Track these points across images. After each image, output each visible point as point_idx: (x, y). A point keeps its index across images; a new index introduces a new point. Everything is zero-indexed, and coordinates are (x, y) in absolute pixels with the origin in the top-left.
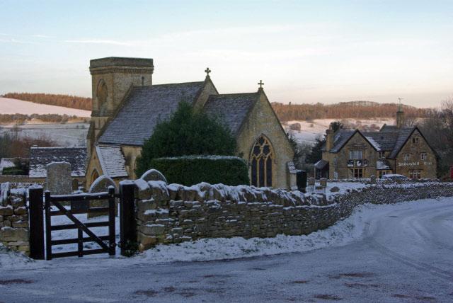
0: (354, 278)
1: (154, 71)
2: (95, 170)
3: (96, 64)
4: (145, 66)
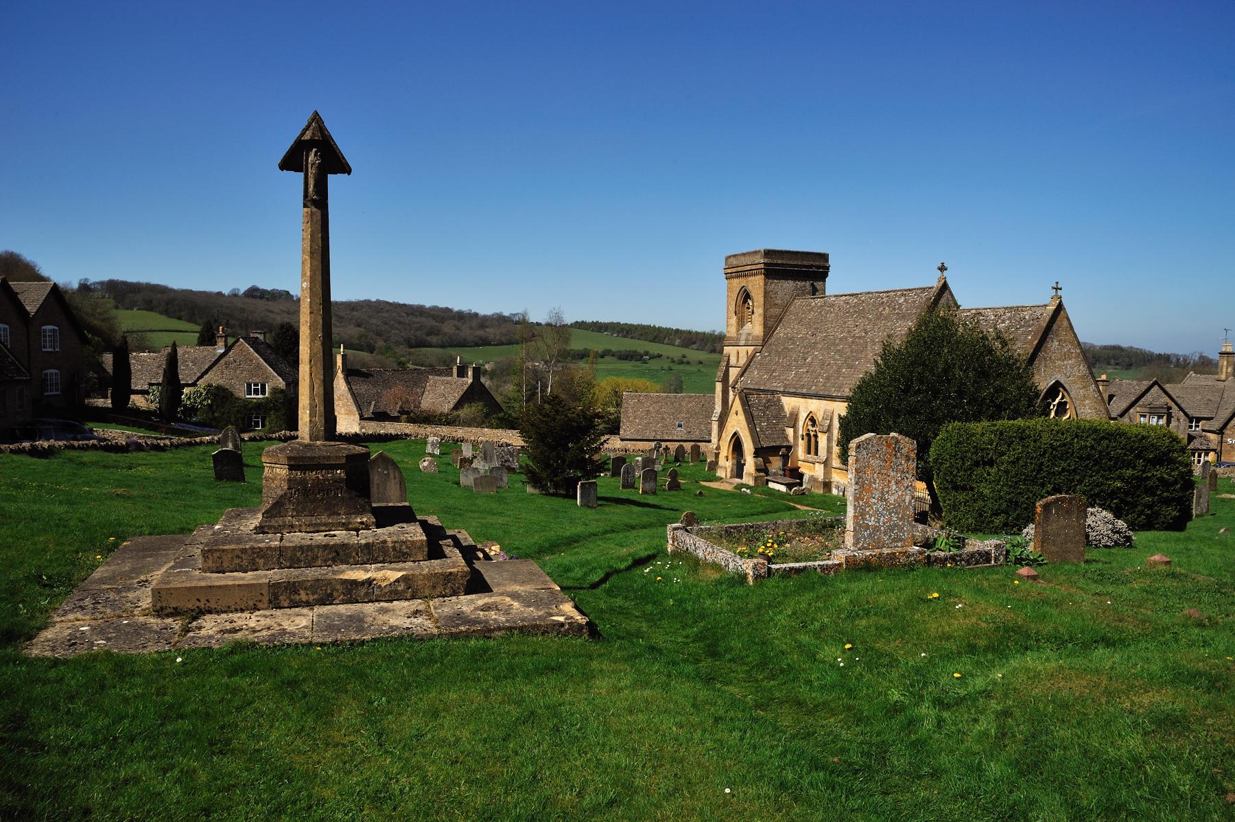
3: (734, 262)
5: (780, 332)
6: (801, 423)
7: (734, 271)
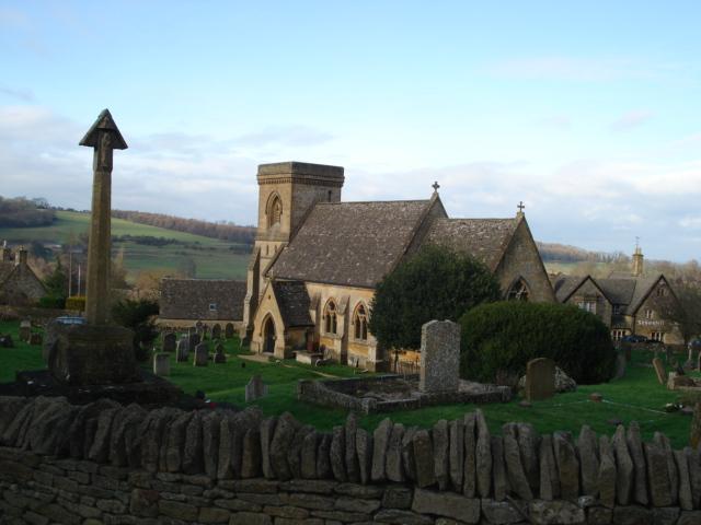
0: (676, 479)
1: (345, 184)
2: (269, 314)
3: (265, 170)
4: (331, 177)
5: (304, 231)
6: (322, 307)
7: (267, 175)
